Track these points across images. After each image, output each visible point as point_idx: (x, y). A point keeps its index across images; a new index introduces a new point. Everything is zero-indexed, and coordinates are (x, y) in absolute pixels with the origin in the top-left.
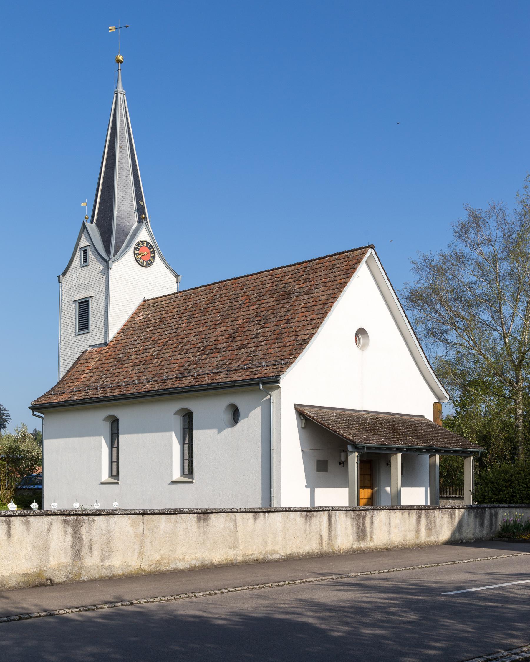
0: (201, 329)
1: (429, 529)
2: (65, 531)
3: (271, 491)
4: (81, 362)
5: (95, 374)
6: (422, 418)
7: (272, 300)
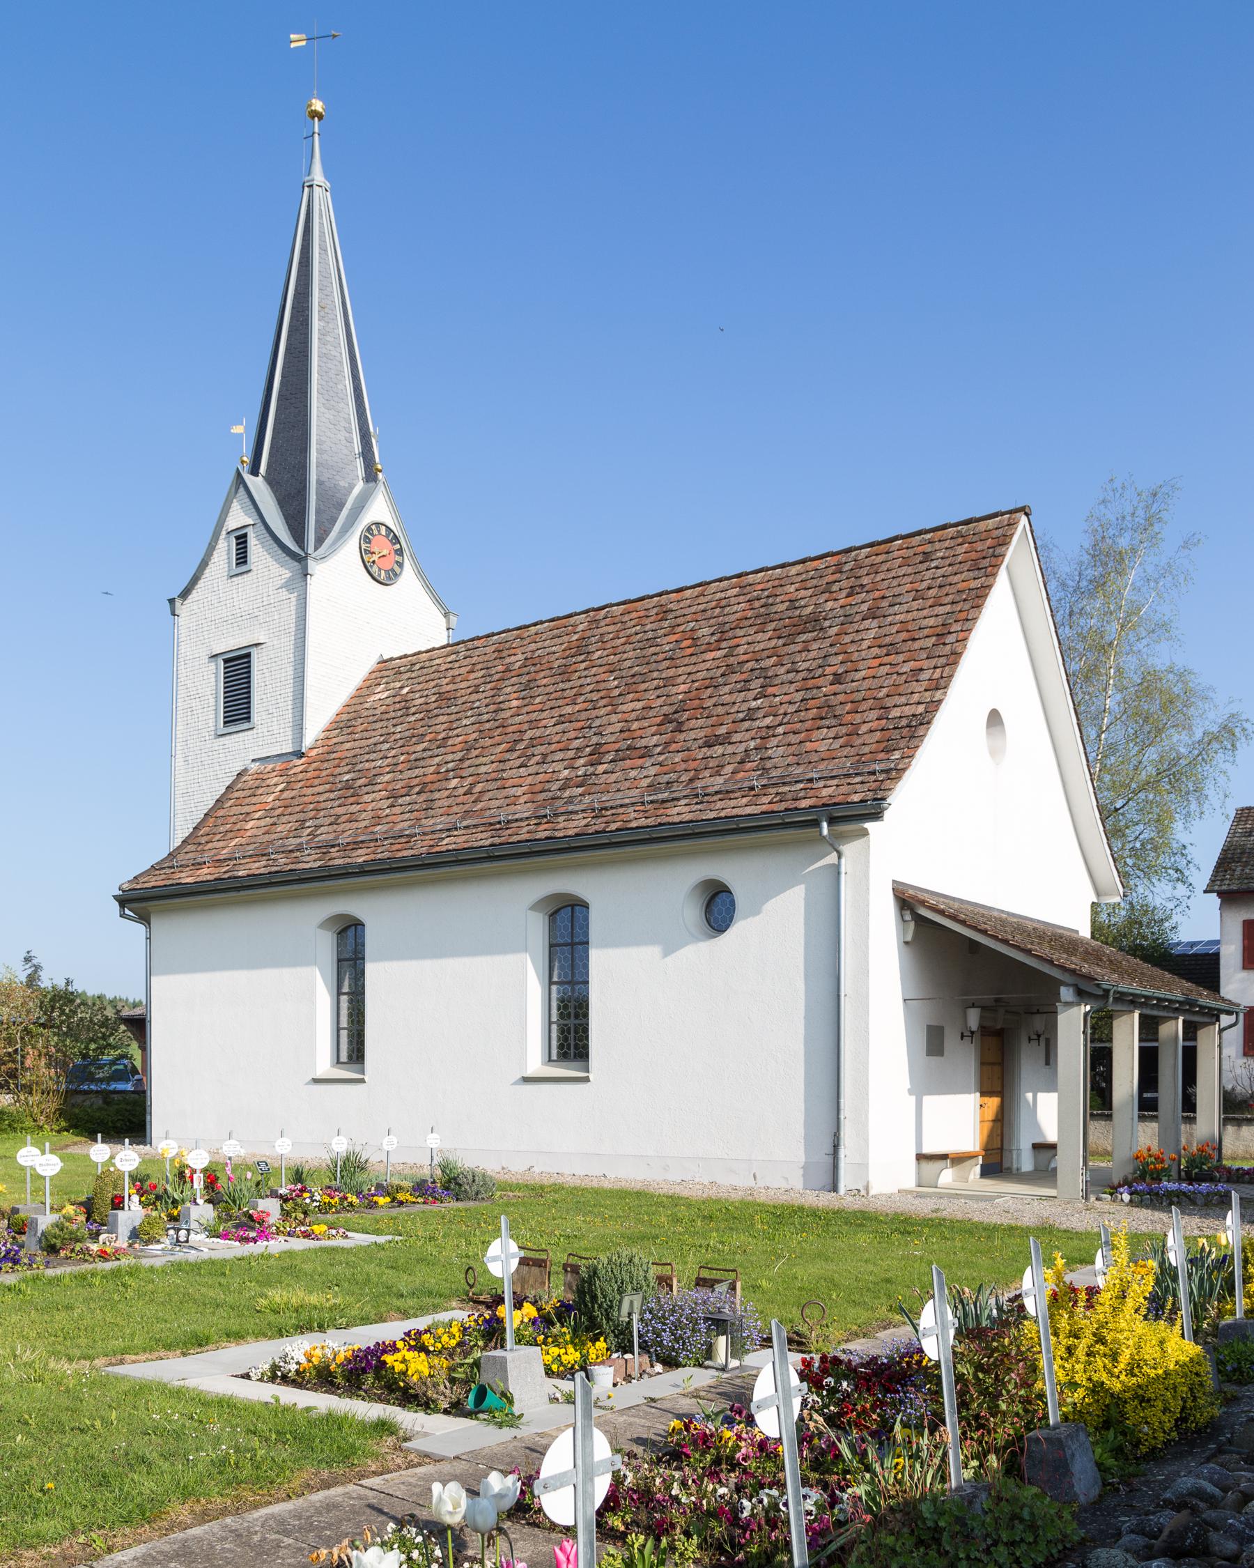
0: (569, 709)
3: (838, 1103)
4: (236, 795)
5: (284, 819)
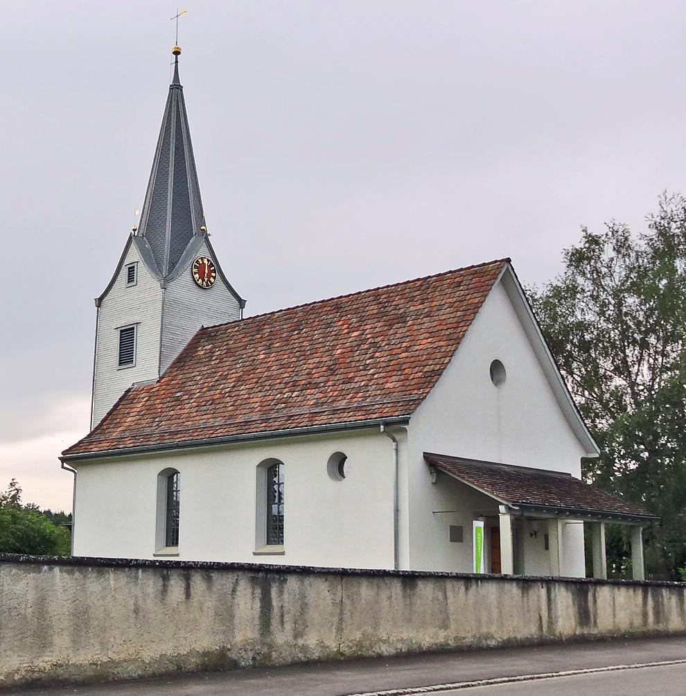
1: (657, 613)
2: (253, 593)
5: (146, 417)
6: (569, 476)
7: (380, 324)
